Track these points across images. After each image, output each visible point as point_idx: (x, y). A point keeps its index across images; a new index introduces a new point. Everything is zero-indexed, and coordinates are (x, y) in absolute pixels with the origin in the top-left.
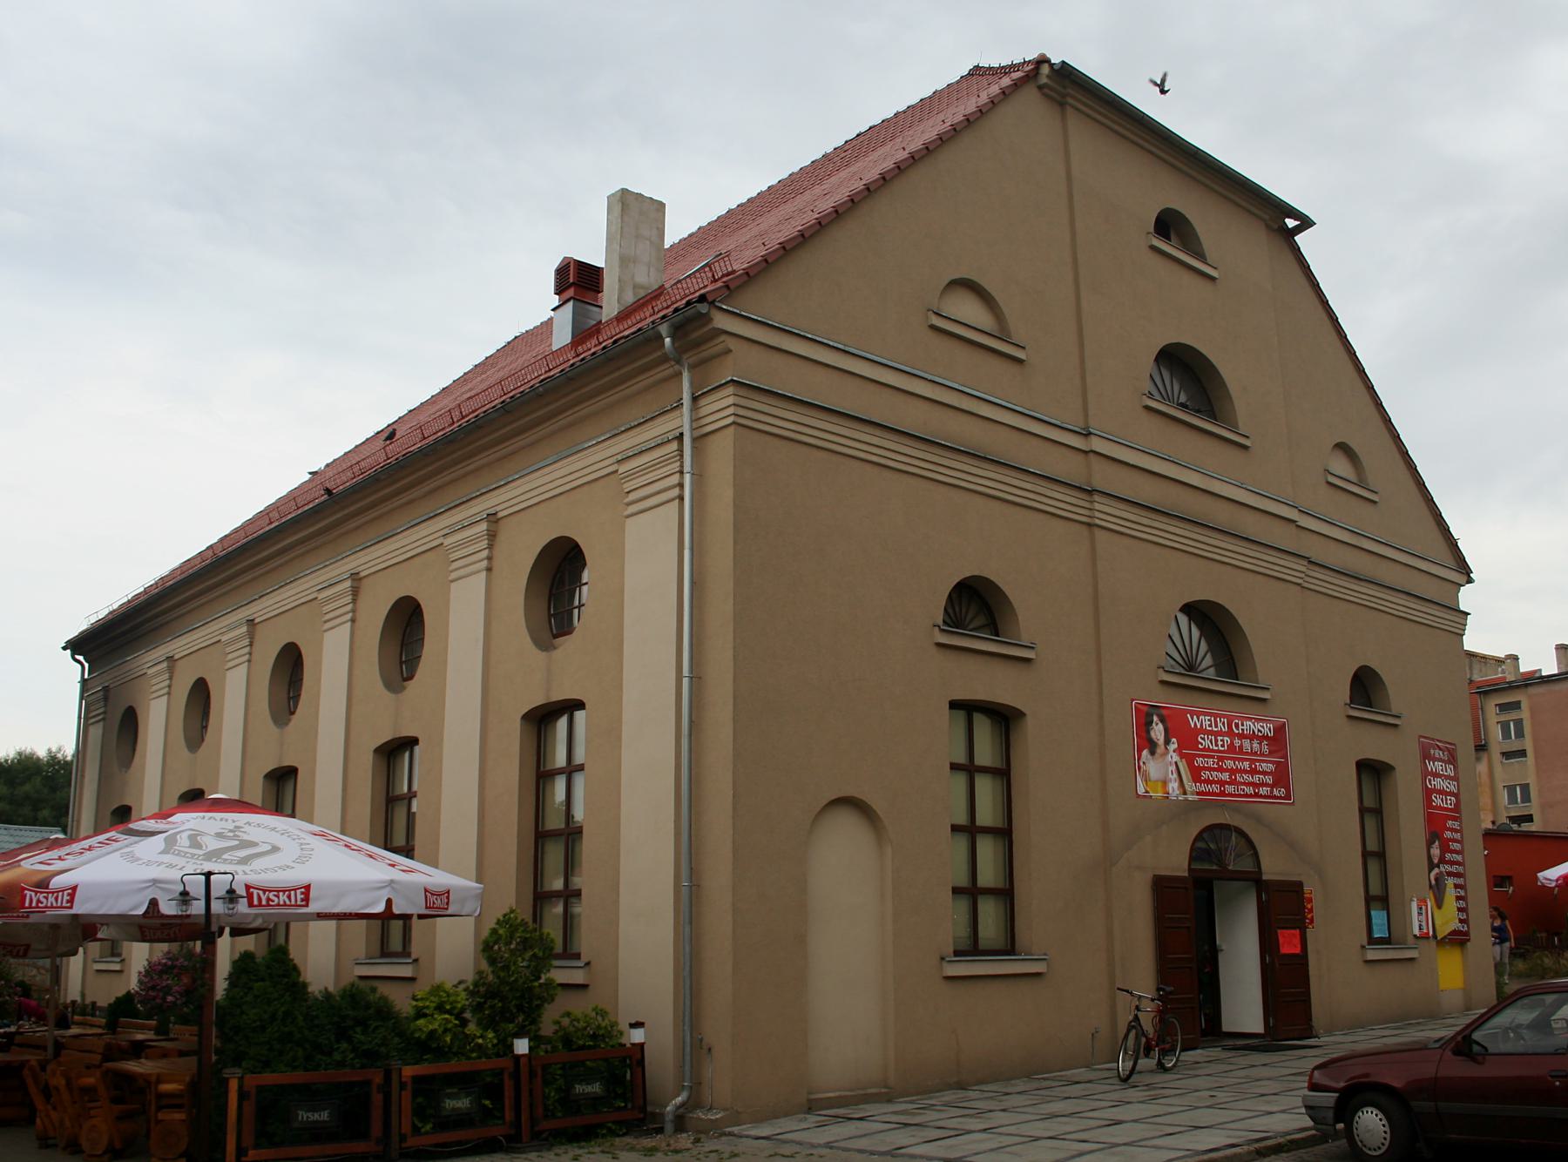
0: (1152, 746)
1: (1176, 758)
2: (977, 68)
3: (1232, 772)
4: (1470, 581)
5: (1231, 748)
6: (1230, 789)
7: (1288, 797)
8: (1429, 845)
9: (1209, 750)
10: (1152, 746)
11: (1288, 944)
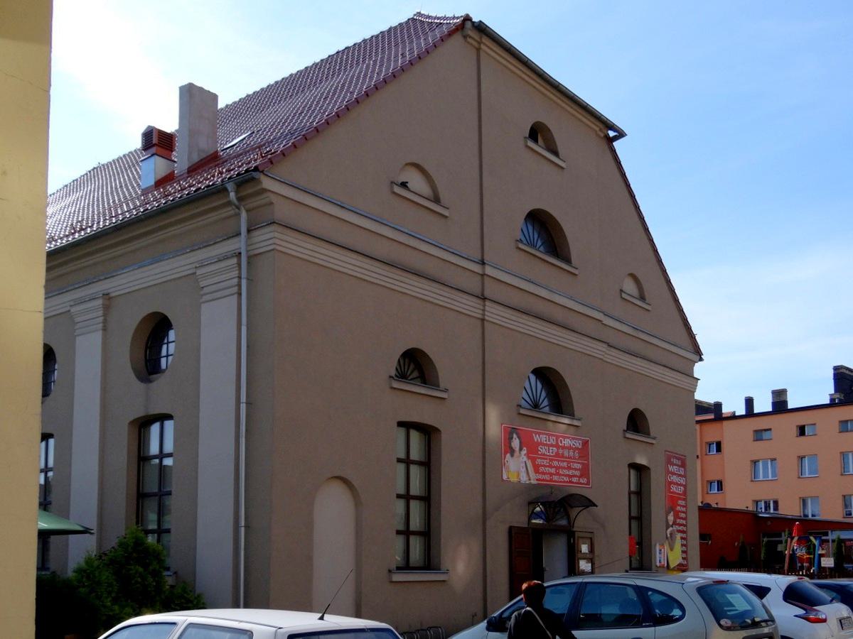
0: (512, 452)
1: (525, 459)
4: (701, 359)
5: (557, 455)
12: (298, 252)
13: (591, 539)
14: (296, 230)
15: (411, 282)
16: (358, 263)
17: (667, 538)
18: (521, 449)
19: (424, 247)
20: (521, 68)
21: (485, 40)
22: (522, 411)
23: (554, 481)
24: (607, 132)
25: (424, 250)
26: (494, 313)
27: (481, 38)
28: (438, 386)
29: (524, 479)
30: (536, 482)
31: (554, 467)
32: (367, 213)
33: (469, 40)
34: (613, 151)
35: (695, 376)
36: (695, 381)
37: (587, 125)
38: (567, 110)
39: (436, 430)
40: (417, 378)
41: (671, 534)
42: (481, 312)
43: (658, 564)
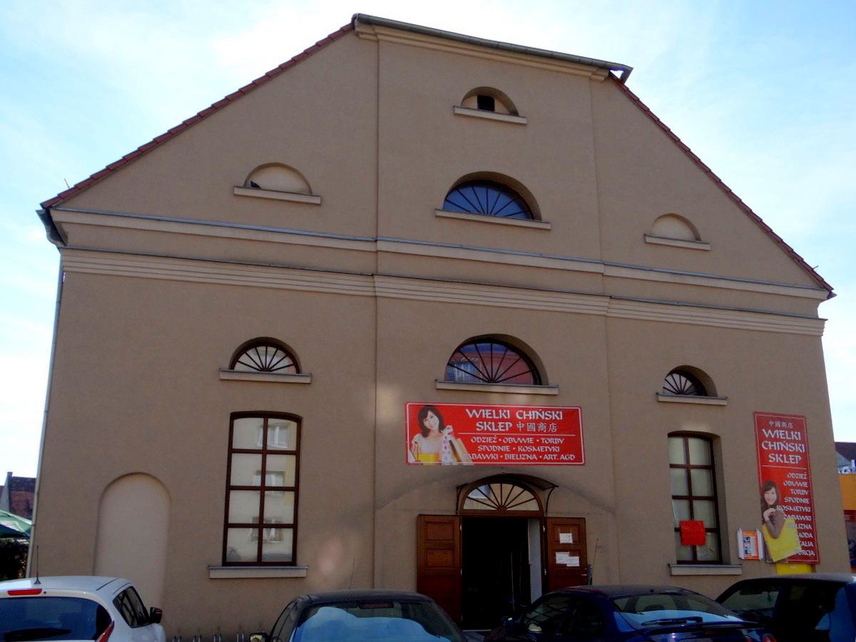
0: (426, 432)
1: (450, 438)
2: (361, 21)
3: (512, 445)
4: (831, 295)
5: (511, 430)
6: (507, 456)
7: (578, 459)
8: (764, 490)
9: (488, 431)
10: (426, 432)
11: (397, 605)
12: (332, 283)
13: (579, 525)
14: (96, 251)
15: (257, 274)
16: (176, 267)
17: (764, 522)
18: (442, 427)
19: (277, 238)
20: (396, 34)
21: (379, 30)
22: (661, 399)
23: (506, 461)
24: (609, 76)
25: (278, 241)
26: (385, 287)
27: (374, 29)
28: (717, 396)
29: (447, 459)
30: (472, 463)
31: (508, 444)
32: (160, 216)
33: (361, 36)
34: (627, 92)
35: (820, 317)
36: (820, 322)
37: (538, 68)
38: (494, 60)
39: (717, 437)
40: (693, 392)
41: (771, 517)
42: (371, 289)
43: (742, 555)
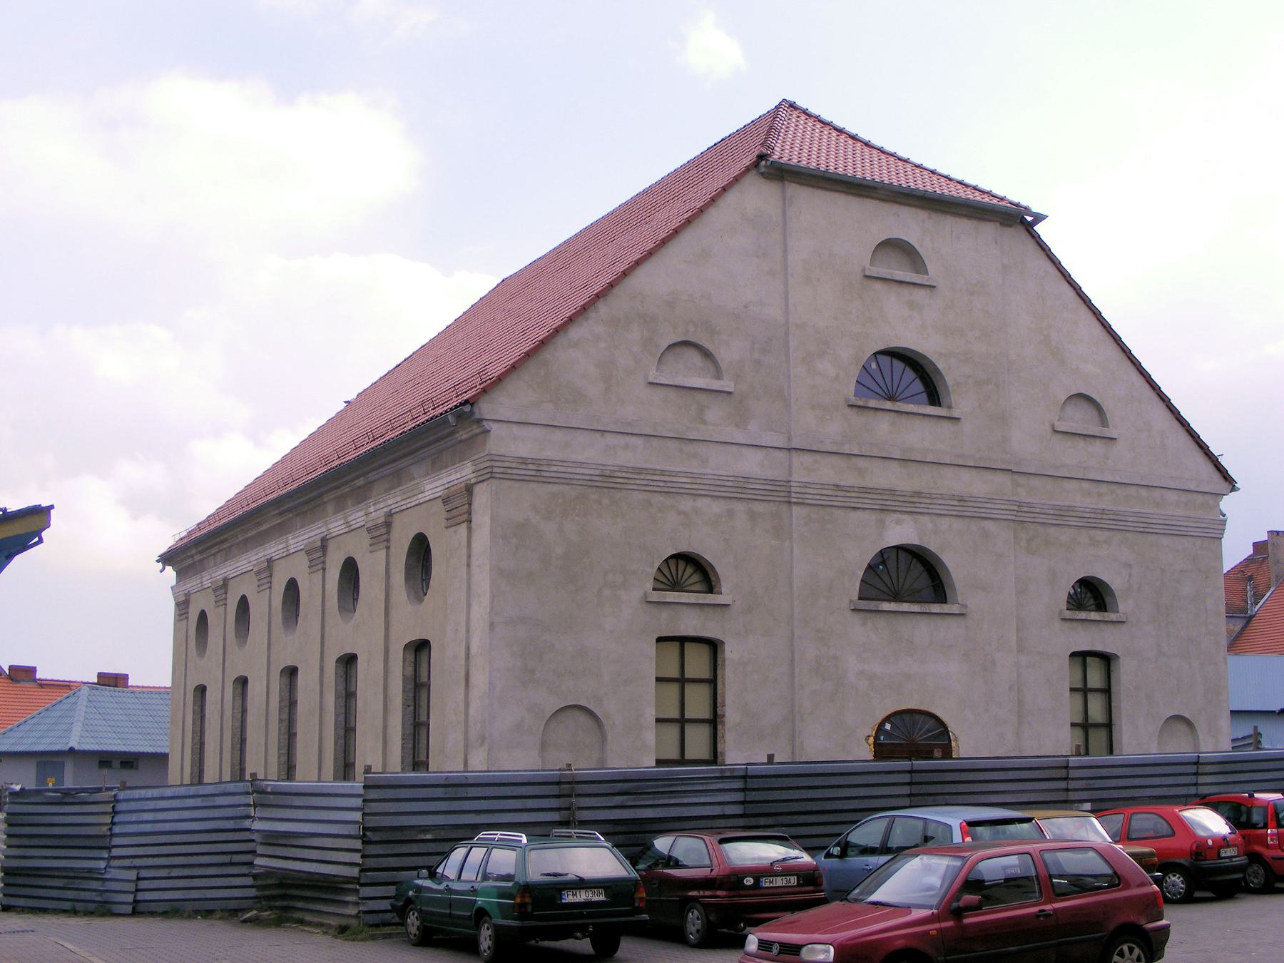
4: (1234, 489)
